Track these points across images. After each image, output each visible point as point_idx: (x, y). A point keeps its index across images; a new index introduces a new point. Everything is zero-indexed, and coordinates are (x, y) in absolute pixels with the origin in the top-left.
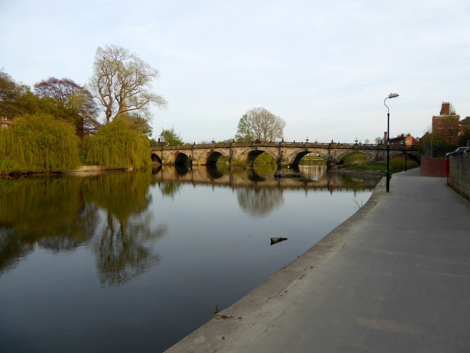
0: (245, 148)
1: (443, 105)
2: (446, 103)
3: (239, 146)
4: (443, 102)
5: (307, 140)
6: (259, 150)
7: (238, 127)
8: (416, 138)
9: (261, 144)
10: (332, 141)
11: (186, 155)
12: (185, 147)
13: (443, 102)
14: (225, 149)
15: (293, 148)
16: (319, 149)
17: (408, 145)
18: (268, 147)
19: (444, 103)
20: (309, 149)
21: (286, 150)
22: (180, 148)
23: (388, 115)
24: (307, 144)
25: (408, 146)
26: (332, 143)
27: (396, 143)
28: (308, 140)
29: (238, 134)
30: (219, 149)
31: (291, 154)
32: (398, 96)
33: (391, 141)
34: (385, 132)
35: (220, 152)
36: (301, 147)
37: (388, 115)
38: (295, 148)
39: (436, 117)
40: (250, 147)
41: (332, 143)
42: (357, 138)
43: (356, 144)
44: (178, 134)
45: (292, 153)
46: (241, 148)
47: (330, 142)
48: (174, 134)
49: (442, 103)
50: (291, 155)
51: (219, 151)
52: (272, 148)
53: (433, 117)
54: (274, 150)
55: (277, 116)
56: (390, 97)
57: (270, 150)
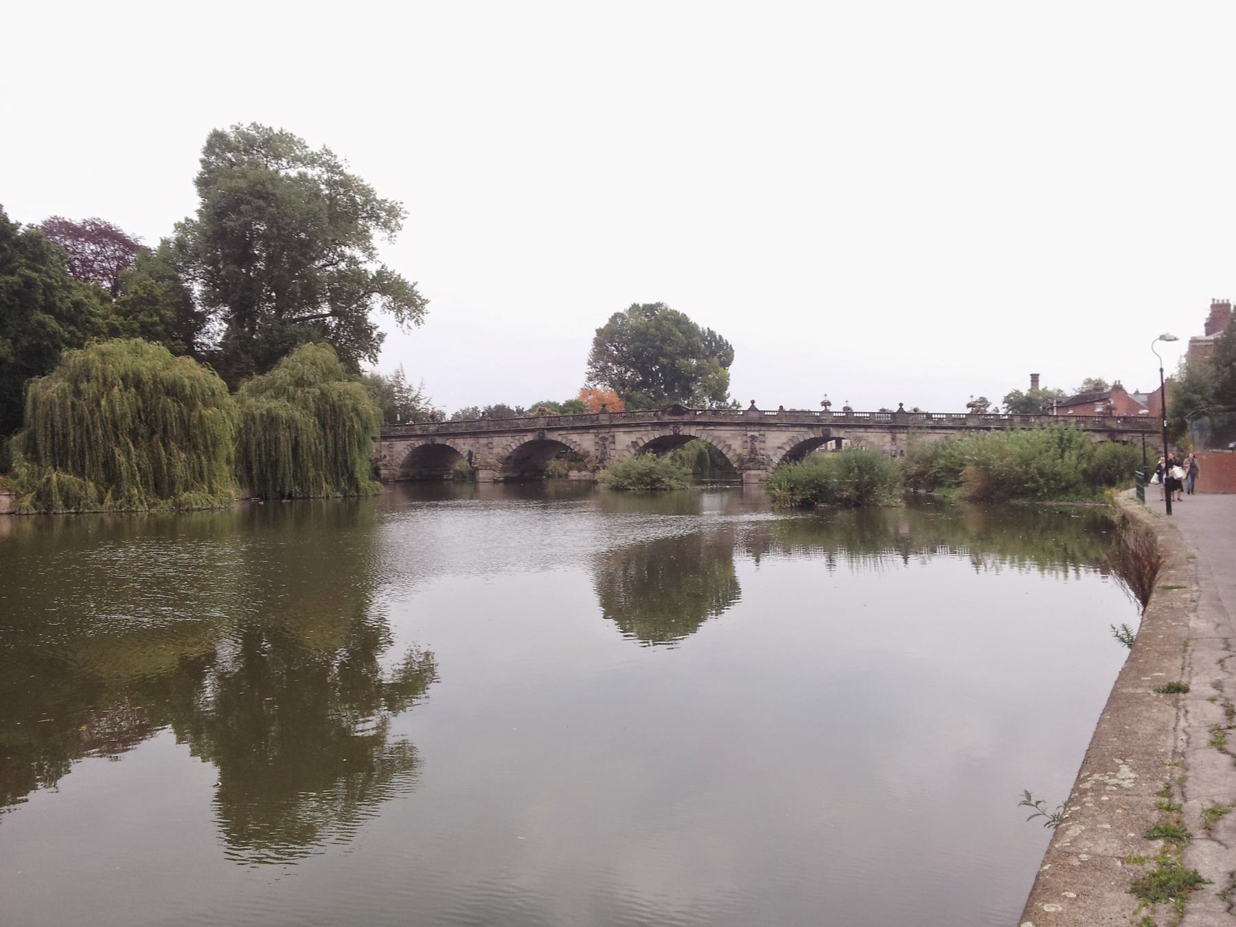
0: (639, 429)
1: (1213, 306)
2: (1220, 302)
3: (621, 422)
4: (1213, 300)
5: (826, 404)
6: (681, 433)
7: (590, 363)
8: (1133, 393)
9: (686, 418)
10: (901, 405)
11: (458, 450)
12: (452, 428)
13: (1213, 300)
14: (579, 431)
15: (783, 429)
16: (862, 430)
17: (856, 413)
18: (710, 425)
19: (1216, 302)
20: (831, 429)
21: (764, 435)
22: (437, 430)
23: (1162, 370)
24: (827, 414)
25: (858, 415)
26: (901, 411)
27: (1081, 411)
28: (830, 405)
29: (591, 384)
30: (561, 432)
31: (780, 445)
32: (1176, 339)
33: (1067, 402)
34: (1032, 375)
35: (451, 446)
36: (810, 426)
37: (1162, 370)
38: (791, 429)
39: (1199, 341)
40: (654, 425)
41: (901, 411)
42: (972, 396)
43: (826, 411)
44: (415, 388)
45: (783, 443)
46: (627, 430)
47: (895, 409)
48: (405, 386)
49: (1211, 303)
50: (779, 448)
51: (559, 439)
52: (723, 428)
53: (1191, 342)
54: (728, 434)
55: (706, 328)
56: (1162, 338)
57: (716, 433)
